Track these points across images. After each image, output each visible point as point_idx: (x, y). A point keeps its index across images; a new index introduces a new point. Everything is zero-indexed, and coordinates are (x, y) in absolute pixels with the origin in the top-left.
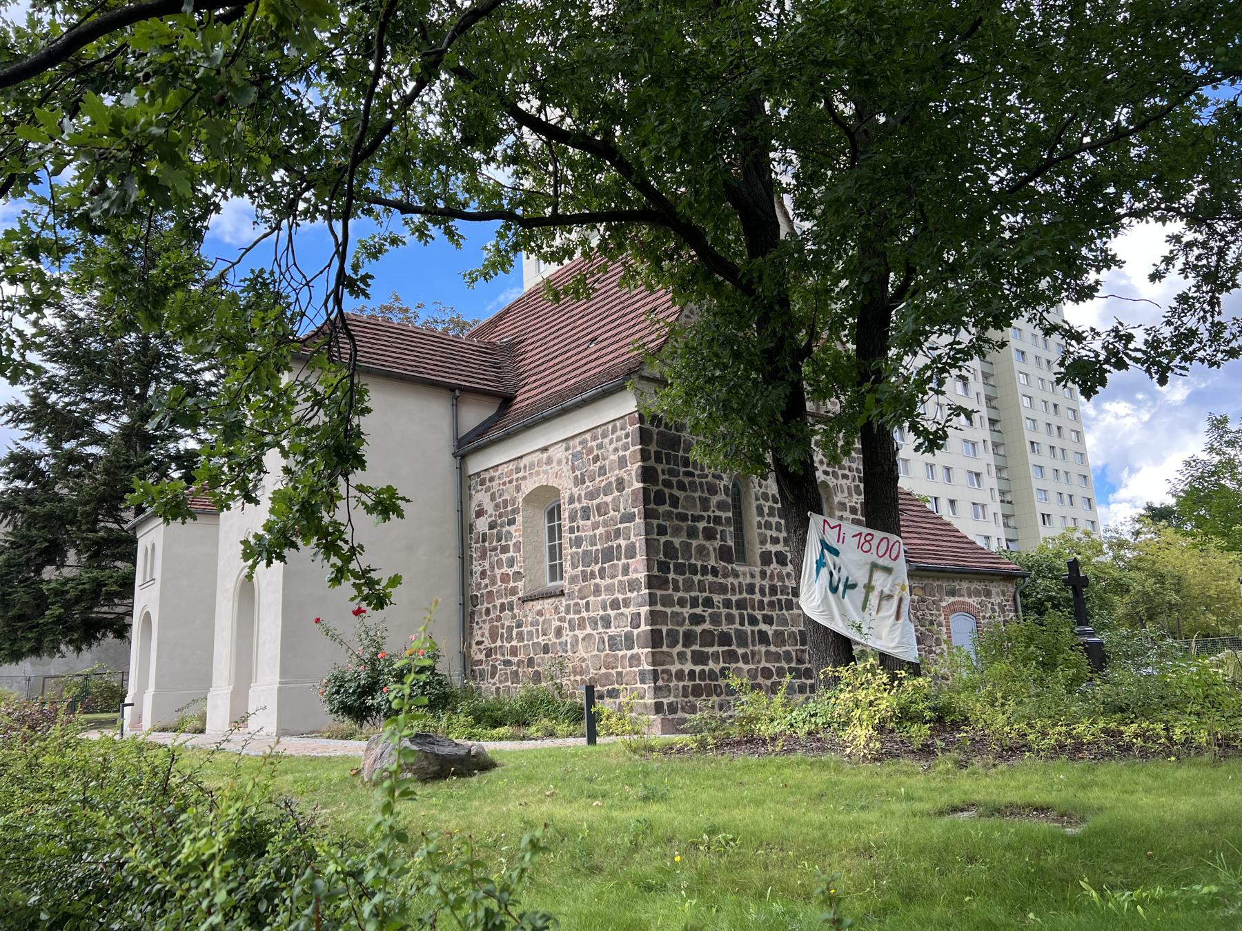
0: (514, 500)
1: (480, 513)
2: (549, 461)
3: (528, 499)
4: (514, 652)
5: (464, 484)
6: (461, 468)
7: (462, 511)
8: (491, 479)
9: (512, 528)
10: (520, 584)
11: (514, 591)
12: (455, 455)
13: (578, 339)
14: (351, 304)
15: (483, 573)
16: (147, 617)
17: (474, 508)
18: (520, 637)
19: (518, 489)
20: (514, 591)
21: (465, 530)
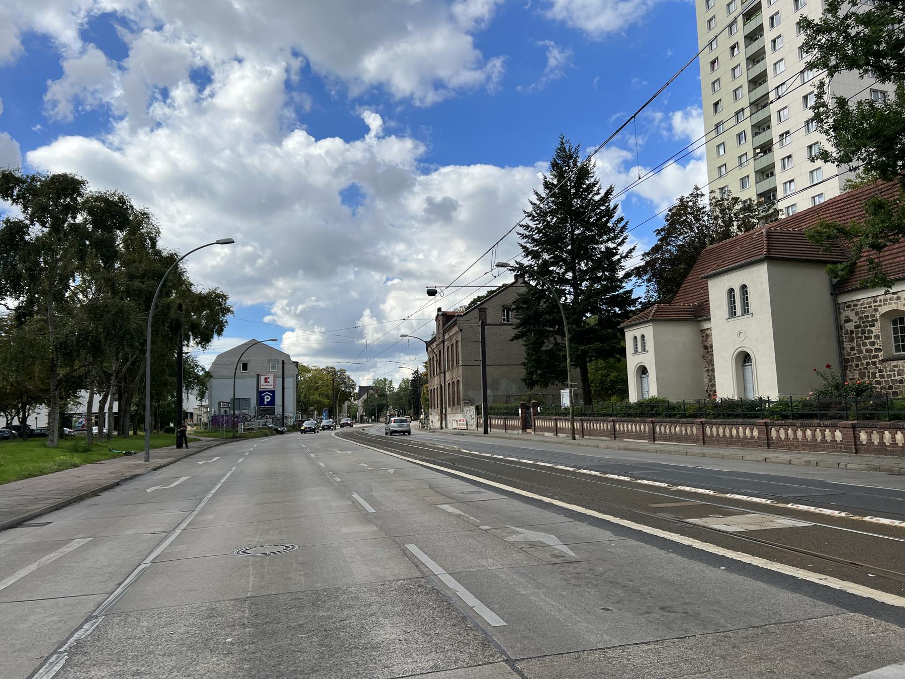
0: (873, 316)
1: (848, 320)
2: (898, 298)
3: (882, 316)
4: (873, 344)
5: (837, 308)
6: (835, 300)
7: (837, 319)
8: (856, 305)
9: (873, 329)
10: (880, 354)
11: (876, 357)
12: (832, 294)
13: (453, 361)
14: (463, 214)
15: (852, 349)
16: (643, 371)
17: (843, 318)
18: (882, 377)
19: (876, 310)
20: (877, 357)
21: (839, 328)
